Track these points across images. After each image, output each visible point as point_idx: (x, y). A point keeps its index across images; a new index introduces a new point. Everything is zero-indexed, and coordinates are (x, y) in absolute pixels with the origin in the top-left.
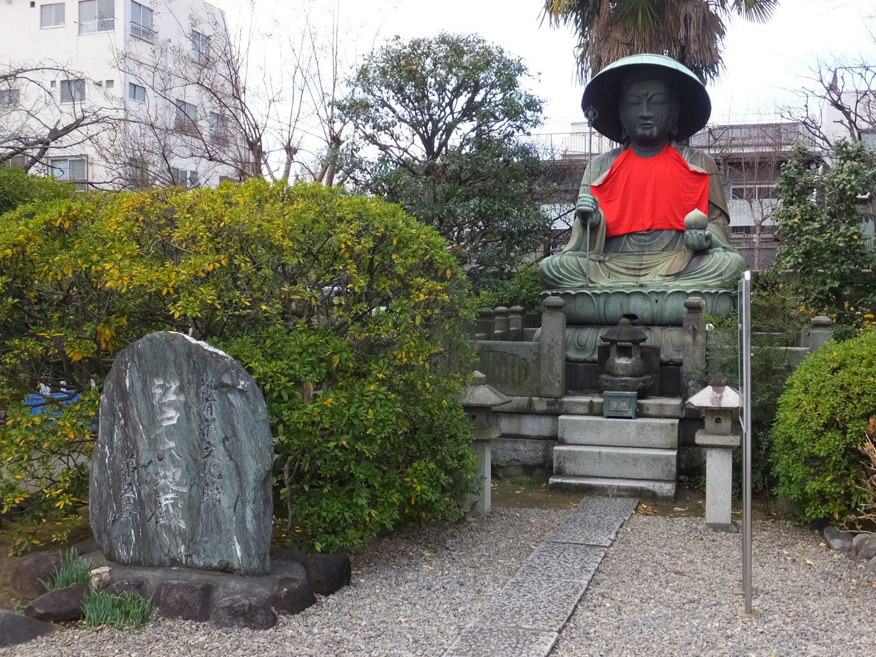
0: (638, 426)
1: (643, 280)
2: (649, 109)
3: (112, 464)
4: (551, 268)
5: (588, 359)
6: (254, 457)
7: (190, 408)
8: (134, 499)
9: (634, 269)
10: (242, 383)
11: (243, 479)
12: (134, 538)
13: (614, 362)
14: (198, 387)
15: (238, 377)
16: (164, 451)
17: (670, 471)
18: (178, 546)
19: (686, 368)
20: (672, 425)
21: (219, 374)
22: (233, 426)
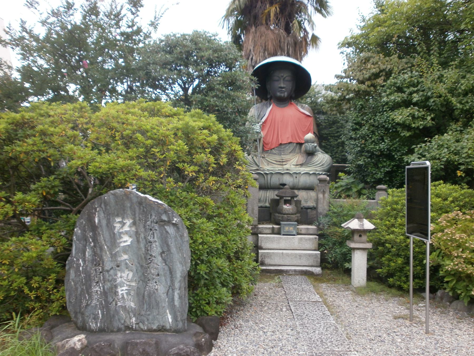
1: (285, 167)
2: (284, 84)
3: (85, 271)
6: (181, 263)
7: (140, 234)
8: (100, 291)
9: (280, 162)
10: (175, 219)
11: (174, 276)
12: (100, 316)
13: (283, 208)
14: (146, 222)
15: (173, 216)
16: (121, 261)
17: (317, 261)
18: (131, 318)
21: (159, 214)
22: (168, 246)
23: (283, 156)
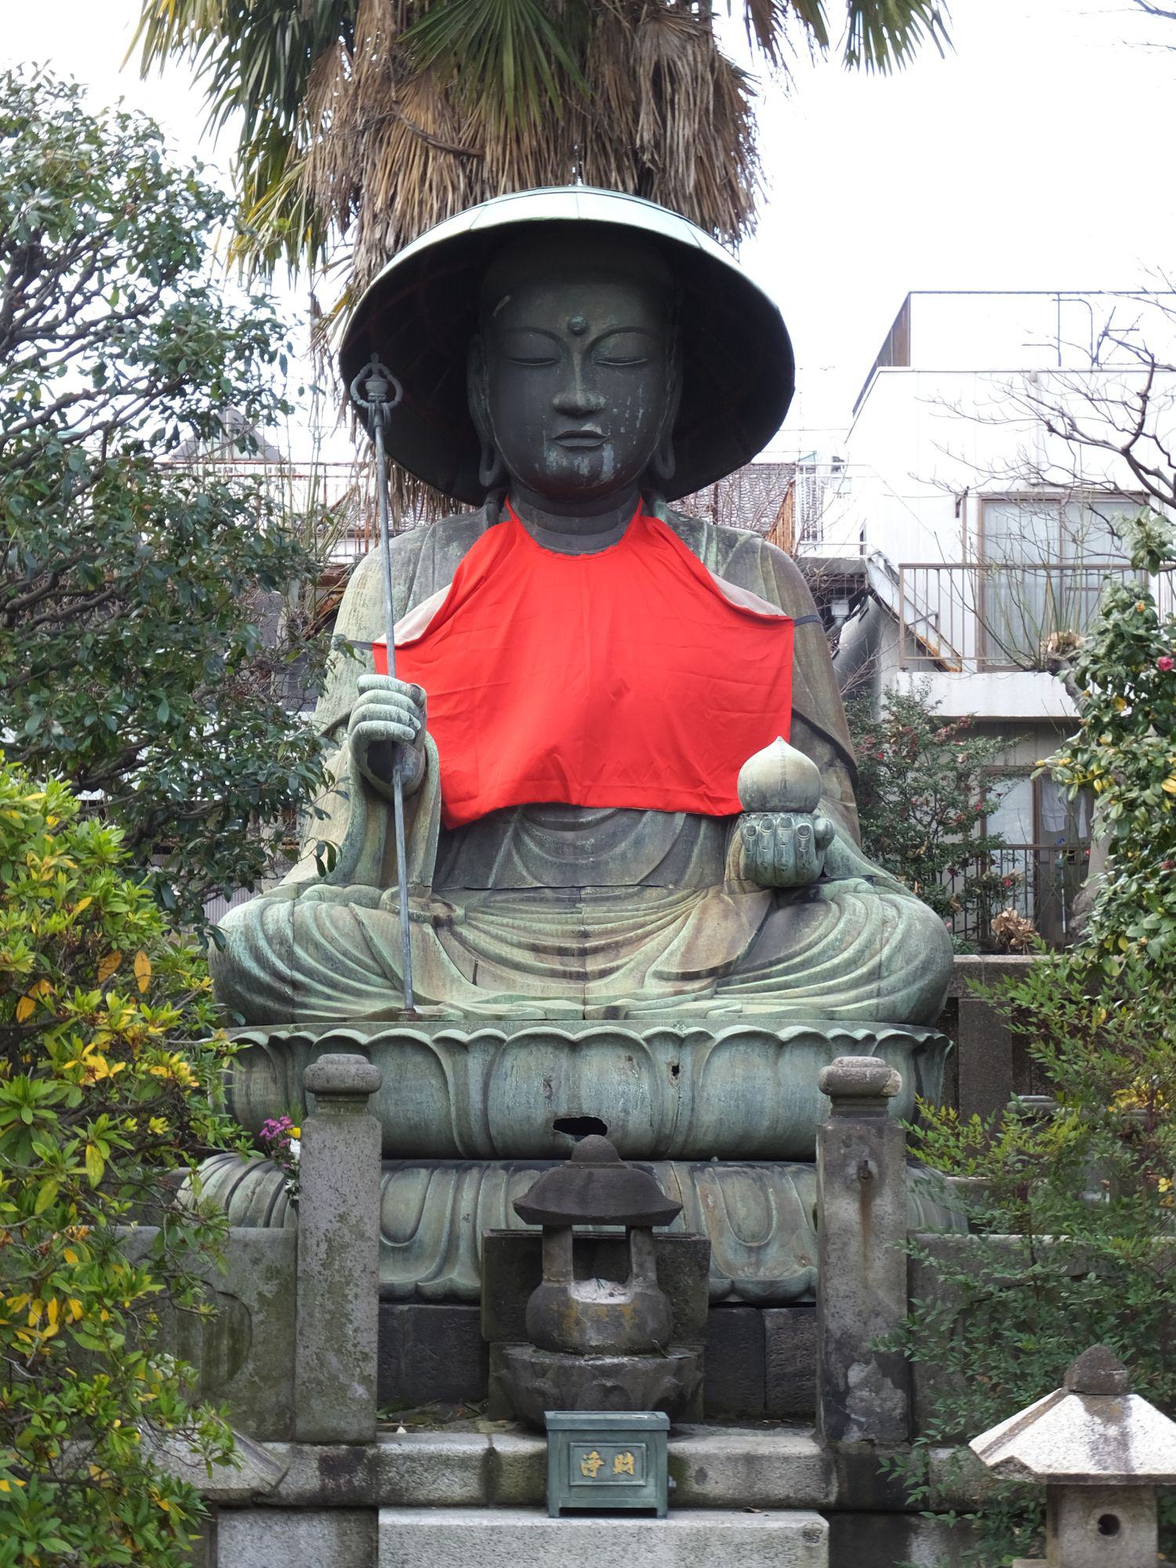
0: (682, 1546)
1: (602, 991)
2: (590, 384)
4: (262, 943)
5: (431, 1286)
9: (562, 952)
13: (568, 1302)
19: (841, 1312)
20: (809, 1535)
23: (587, 911)
